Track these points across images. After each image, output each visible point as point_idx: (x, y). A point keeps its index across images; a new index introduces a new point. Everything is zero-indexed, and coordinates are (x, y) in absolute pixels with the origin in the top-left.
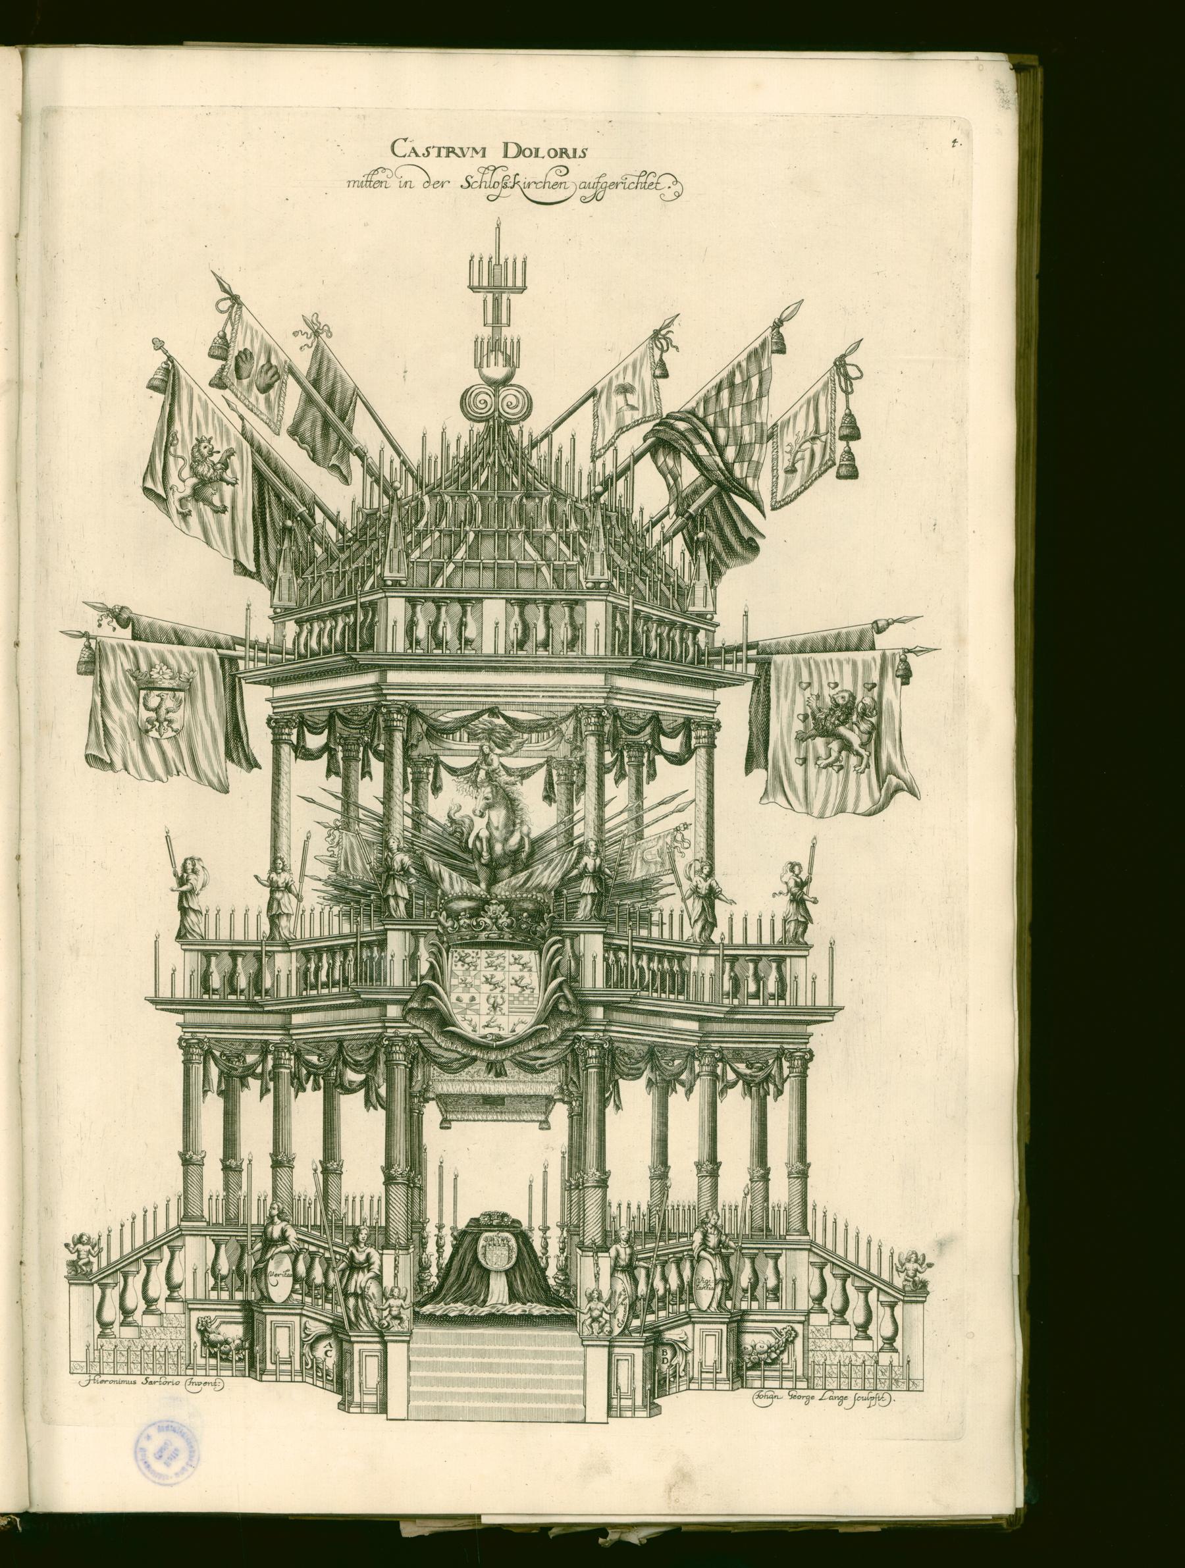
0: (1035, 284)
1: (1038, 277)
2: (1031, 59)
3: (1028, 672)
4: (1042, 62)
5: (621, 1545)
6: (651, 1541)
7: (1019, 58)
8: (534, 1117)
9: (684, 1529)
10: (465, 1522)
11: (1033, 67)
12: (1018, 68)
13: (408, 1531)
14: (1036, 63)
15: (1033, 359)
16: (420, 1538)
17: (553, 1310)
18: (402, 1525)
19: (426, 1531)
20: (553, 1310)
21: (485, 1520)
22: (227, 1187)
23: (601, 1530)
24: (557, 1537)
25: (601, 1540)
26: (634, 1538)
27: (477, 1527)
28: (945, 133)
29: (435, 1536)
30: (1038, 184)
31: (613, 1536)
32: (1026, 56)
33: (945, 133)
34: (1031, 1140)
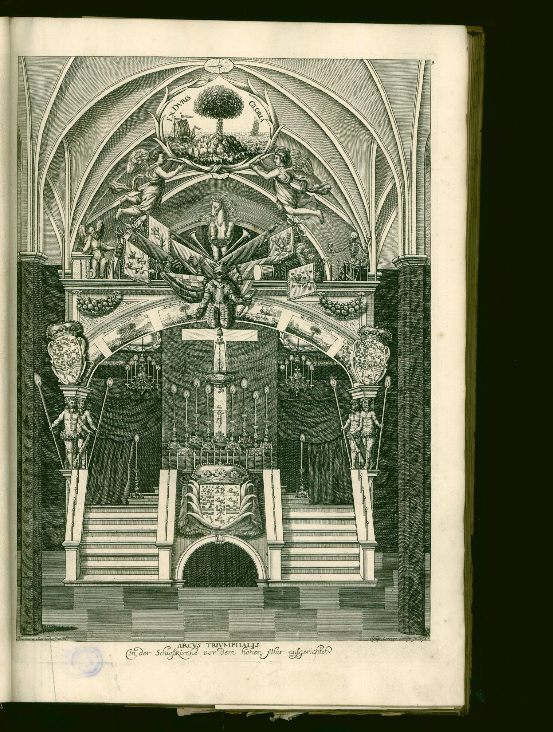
0: (480, 135)
1: (481, 131)
2: (479, 29)
3: (475, 315)
4: (484, 31)
5: (280, 720)
6: (294, 719)
7: (472, 28)
8: (274, 585)
9: (310, 713)
10: (207, 709)
11: (480, 33)
12: (471, 34)
13: (181, 713)
14: (481, 31)
15: (479, 169)
16: (186, 716)
17: (238, 261)
18: (178, 710)
19: (189, 713)
20: (238, 261)
21: (217, 707)
22: (174, 540)
23: (271, 713)
24: (251, 716)
25: (271, 718)
26: (286, 717)
27: (213, 712)
28: (444, 53)
29: (194, 715)
30: (482, 87)
31: (276, 716)
32: (477, 27)
33: (444, 53)
34: (475, 532)
